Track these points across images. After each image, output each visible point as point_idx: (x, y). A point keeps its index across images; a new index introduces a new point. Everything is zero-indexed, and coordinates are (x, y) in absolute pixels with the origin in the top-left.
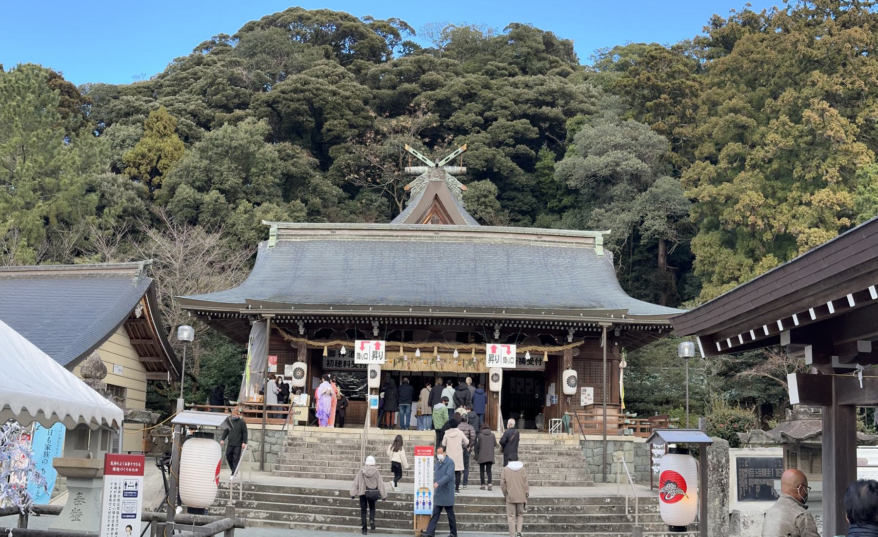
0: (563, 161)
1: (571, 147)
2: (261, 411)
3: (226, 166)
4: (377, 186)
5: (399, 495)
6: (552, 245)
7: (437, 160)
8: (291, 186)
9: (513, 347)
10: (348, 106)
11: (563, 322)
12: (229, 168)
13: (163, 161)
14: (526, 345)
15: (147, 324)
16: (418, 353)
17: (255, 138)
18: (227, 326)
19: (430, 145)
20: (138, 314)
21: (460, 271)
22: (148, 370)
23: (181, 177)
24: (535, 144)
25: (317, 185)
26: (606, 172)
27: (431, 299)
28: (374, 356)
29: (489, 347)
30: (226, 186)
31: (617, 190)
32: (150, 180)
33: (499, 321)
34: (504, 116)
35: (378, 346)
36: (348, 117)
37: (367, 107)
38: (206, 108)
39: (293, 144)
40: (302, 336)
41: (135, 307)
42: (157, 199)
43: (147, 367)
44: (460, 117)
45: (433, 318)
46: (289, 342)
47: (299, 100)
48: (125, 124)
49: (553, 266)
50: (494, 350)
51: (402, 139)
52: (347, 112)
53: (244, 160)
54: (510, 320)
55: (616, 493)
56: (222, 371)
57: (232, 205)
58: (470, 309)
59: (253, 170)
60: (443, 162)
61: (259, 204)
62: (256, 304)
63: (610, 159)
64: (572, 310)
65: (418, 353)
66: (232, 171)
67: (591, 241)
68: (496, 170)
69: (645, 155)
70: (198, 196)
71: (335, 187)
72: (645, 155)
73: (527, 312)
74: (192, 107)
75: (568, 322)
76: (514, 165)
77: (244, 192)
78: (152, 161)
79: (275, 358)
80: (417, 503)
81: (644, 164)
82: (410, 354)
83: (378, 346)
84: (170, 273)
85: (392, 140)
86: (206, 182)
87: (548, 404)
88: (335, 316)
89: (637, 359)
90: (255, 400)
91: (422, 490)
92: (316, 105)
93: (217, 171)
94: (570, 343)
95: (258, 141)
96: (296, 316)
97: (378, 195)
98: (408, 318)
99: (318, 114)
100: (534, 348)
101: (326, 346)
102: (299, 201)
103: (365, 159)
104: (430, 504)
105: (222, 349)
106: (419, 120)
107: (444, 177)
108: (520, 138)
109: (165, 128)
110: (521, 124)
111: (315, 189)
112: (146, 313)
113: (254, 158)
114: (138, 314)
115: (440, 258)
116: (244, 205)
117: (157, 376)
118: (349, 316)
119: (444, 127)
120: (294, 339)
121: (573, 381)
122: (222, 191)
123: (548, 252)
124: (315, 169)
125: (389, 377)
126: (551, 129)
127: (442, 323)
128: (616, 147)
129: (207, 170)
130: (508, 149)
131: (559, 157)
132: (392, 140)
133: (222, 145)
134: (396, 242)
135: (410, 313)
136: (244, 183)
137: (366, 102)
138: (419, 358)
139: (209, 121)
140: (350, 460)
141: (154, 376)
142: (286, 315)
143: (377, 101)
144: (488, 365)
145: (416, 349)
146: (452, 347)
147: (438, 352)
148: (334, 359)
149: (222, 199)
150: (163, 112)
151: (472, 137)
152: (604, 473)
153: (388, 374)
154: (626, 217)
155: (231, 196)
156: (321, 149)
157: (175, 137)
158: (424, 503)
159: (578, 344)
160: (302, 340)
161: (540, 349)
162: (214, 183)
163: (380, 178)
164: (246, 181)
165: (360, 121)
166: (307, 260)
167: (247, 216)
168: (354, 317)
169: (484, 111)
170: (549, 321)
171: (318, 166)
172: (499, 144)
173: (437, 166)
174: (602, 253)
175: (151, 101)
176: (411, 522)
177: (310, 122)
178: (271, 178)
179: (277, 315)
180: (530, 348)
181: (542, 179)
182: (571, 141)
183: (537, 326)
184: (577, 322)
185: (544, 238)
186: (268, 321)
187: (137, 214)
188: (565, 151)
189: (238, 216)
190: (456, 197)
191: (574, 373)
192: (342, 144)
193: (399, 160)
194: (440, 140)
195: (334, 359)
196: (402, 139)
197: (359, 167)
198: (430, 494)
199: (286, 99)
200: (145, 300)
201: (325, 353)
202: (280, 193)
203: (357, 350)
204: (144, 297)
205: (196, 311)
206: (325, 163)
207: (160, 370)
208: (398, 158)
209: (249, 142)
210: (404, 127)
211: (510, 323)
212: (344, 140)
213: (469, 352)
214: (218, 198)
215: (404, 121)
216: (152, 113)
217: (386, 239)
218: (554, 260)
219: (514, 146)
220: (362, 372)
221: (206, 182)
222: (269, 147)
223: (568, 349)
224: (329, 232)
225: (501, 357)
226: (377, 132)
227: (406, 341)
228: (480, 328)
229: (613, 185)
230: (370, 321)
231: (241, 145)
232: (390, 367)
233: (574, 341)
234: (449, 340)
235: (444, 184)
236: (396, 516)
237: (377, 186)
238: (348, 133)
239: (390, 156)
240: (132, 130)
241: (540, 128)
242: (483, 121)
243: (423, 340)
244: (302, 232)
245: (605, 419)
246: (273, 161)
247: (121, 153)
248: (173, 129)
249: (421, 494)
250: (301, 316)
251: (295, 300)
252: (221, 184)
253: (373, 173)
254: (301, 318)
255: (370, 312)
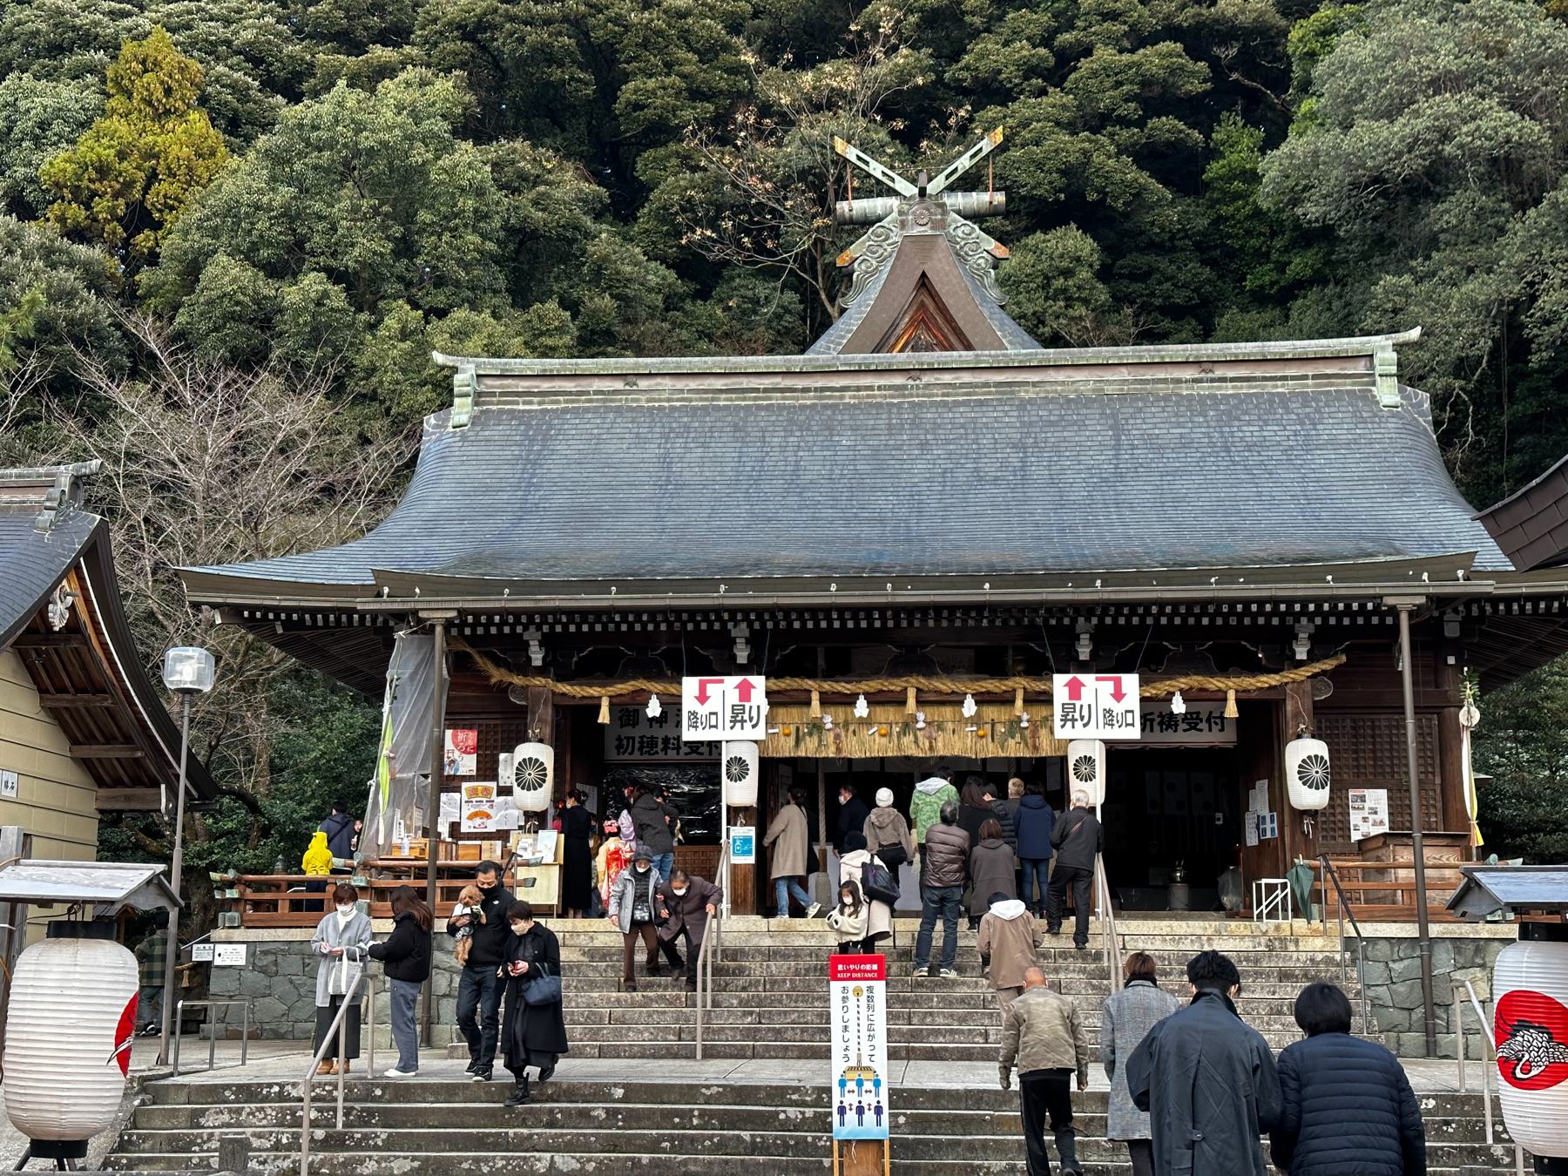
0: (1284, 148)
1: (1307, 105)
2: (424, 883)
3: (345, 204)
4: (768, 261)
5: (796, 1090)
6: (1244, 388)
7: (923, 177)
8: (530, 265)
9: (1131, 682)
10: (685, 37)
11: (1276, 601)
12: (355, 209)
13: (163, 187)
14: (1171, 674)
15: (90, 649)
16: (861, 708)
17: (426, 125)
18: (334, 650)
19: (909, 140)
20: (58, 616)
21: (980, 479)
22: (100, 783)
23: (215, 233)
24: (1199, 111)
25: (605, 259)
26: (1413, 164)
27: (897, 556)
28: (737, 718)
29: (1060, 682)
30: (349, 261)
31: (1447, 213)
32: (126, 243)
33: (1086, 609)
34: (1113, 40)
35: (745, 692)
36: (687, 69)
37: (738, 41)
38: (287, 40)
39: (534, 146)
40: (541, 671)
41: (46, 600)
42: (148, 295)
43: (98, 774)
44: (992, 54)
45: (897, 609)
46: (503, 689)
47: (548, 22)
48: (48, 76)
49: (1249, 448)
50: (1075, 690)
51: (832, 126)
52: (682, 54)
53: (398, 186)
54: (1119, 605)
55: (1456, 1084)
56: (337, 779)
57: (364, 317)
58: (1000, 578)
59: (424, 216)
60: (939, 182)
61: (442, 314)
62: (402, 582)
63: (1420, 124)
64: (1303, 567)
65: (861, 708)
66: (364, 218)
67: (1360, 368)
68: (1092, 197)
69: (1529, 94)
70: (267, 288)
71: (653, 264)
72: (1529, 94)
73: (1165, 579)
74: (248, 35)
75: (1290, 602)
76: (1144, 178)
77: (401, 279)
78: (129, 185)
79: (471, 737)
80: (842, 1111)
81: (1528, 122)
82: (841, 712)
83: (745, 692)
84: (178, 507)
85: (805, 131)
86: (289, 251)
87: (1252, 840)
88: (624, 612)
89: (1533, 705)
90: (406, 853)
91: (855, 1075)
92: (597, 35)
93: (321, 218)
94: (1301, 664)
95: (435, 136)
96: (518, 613)
97: (762, 279)
98: (827, 610)
99: (605, 61)
100: (1195, 681)
101: (604, 699)
102: (552, 305)
103: (735, 186)
104: (878, 1111)
105: (337, 719)
106: (881, 70)
107: (942, 224)
108: (1157, 97)
109: (168, 92)
110: (1158, 58)
111: (598, 272)
112: (84, 616)
113: (427, 183)
114: (58, 616)
115: (924, 445)
116: (399, 314)
117: (128, 798)
118: (664, 611)
119: (947, 86)
120: (518, 680)
121: (1317, 772)
122: (335, 276)
123: (1233, 410)
124: (598, 217)
125: (783, 777)
126: (1246, 61)
127: (924, 620)
128: (1440, 83)
129: (289, 216)
130: (1124, 134)
131: (1274, 139)
132: (805, 131)
133: (331, 145)
134: (803, 407)
135: (833, 595)
136: (397, 254)
137: (735, 28)
138: (866, 722)
139: (299, 76)
140: (671, 1003)
141: (117, 798)
142: (490, 613)
143: (765, 23)
144: (1060, 733)
145: (855, 696)
146: (958, 687)
147: (823, 703)
148: (636, 732)
149: (338, 297)
150: (161, 44)
151: (1022, 107)
152: (1430, 1031)
153: (785, 770)
154: (1478, 288)
155: (363, 288)
156: (617, 158)
157: (198, 120)
158: (860, 1111)
159: (1328, 665)
160: (538, 681)
161: (1215, 683)
162: (312, 253)
163: (778, 236)
164: (406, 248)
165: (720, 80)
166: (551, 457)
167: (407, 345)
168: (678, 611)
169: (1057, 31)
170: (1233, 602)
171: (606, 208)
172: (1098, 122)
173: (923, 192)
174: (1395, 399)
175: (128, 14)
176: (826, 1162)
177: (582, 82)
178: (473, 238)
179: (462, 612)
180: (1183, 682)
181: (1225, 210)
182: (1306, 87)
183: (1198, 618)
184: (1319, 601)
185: (1219, 372)
186: (439, 629)
187: (85, 336)
188: (1290, 121)
189: (383, 346)
190: (976, 277)
191: (1319, 748)
192: (673, 146)
193: (825, 182)
194: (934, 124)
195: (636, 732)
196: (832, 126)
197: (720, 208)
198: (877, 1083)
199: (512, 19)
200: (81, 579)
201: (604, 717)
202: (502, 283)
203: (689, 703)
204: (78, 568)
205: (238, 609)
206: (624, 201)
207: (136, 782)
208: (822, 178)
209: (410, 138)
210: (840, 93)
211: (1133, 612)
212: (675, 133)
213: (1006, 700)
214: (325, 295)
215: (839, 75)
216: (128, 48)
217: (776, 399)
218: (1251, 431)
219: (1140, 123)
220: (706, 762)
221: (289, 251)
222: (466, 151)
223: (1299, 679)
224: (619, 385)
225: (1095, 714)
226: (766, 110)
227: (829, 675)
228: (1033, 632)
229: (1438, 198)
230: (724, 624)
231: (384, 144)
232: (786, 748)
233: (1313, 657)
234: (949, 670)
235: (943, 243)
236: (785, 1148)
237: (768, 261)
238: (688, 114)
239: (803, 174)
240: (67, 92)
241: (1214, 63)
242: (1052, 61)
243: (875, 673)
244: (545, 385)
245: (1420, 876)
246: (480, 192)
247: (35, 159)
248: (192, 96)
249: (851, 1085)
250: (530, 613)
251: (518, 571)
252: (334, 255)
253: (759, 223)
254: (531, 621)
255: (722, 596)
